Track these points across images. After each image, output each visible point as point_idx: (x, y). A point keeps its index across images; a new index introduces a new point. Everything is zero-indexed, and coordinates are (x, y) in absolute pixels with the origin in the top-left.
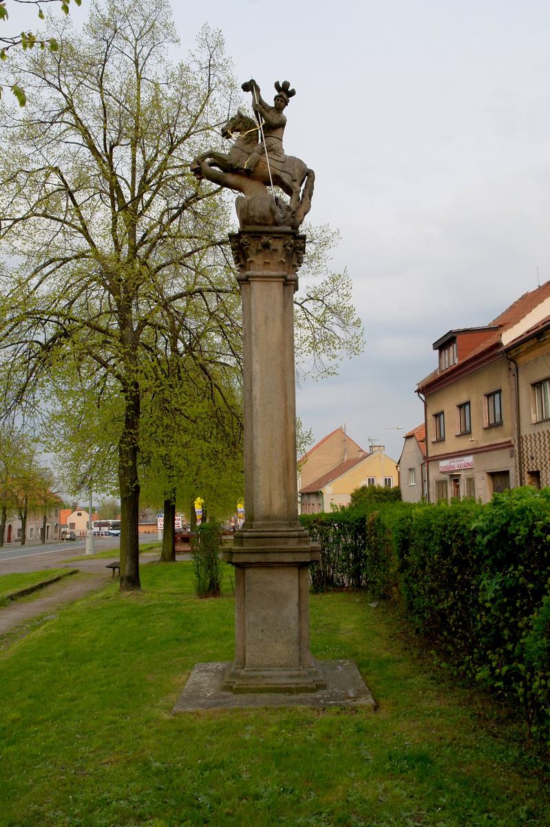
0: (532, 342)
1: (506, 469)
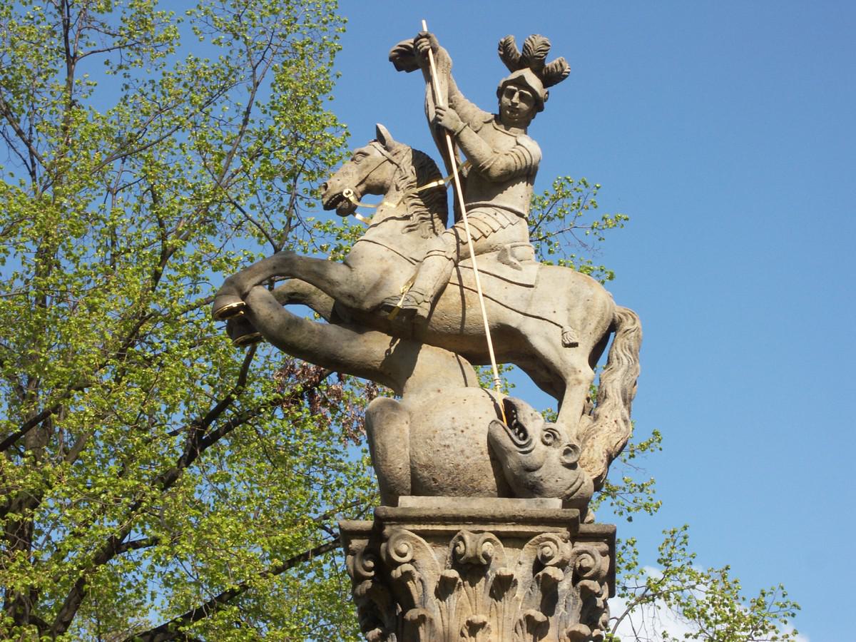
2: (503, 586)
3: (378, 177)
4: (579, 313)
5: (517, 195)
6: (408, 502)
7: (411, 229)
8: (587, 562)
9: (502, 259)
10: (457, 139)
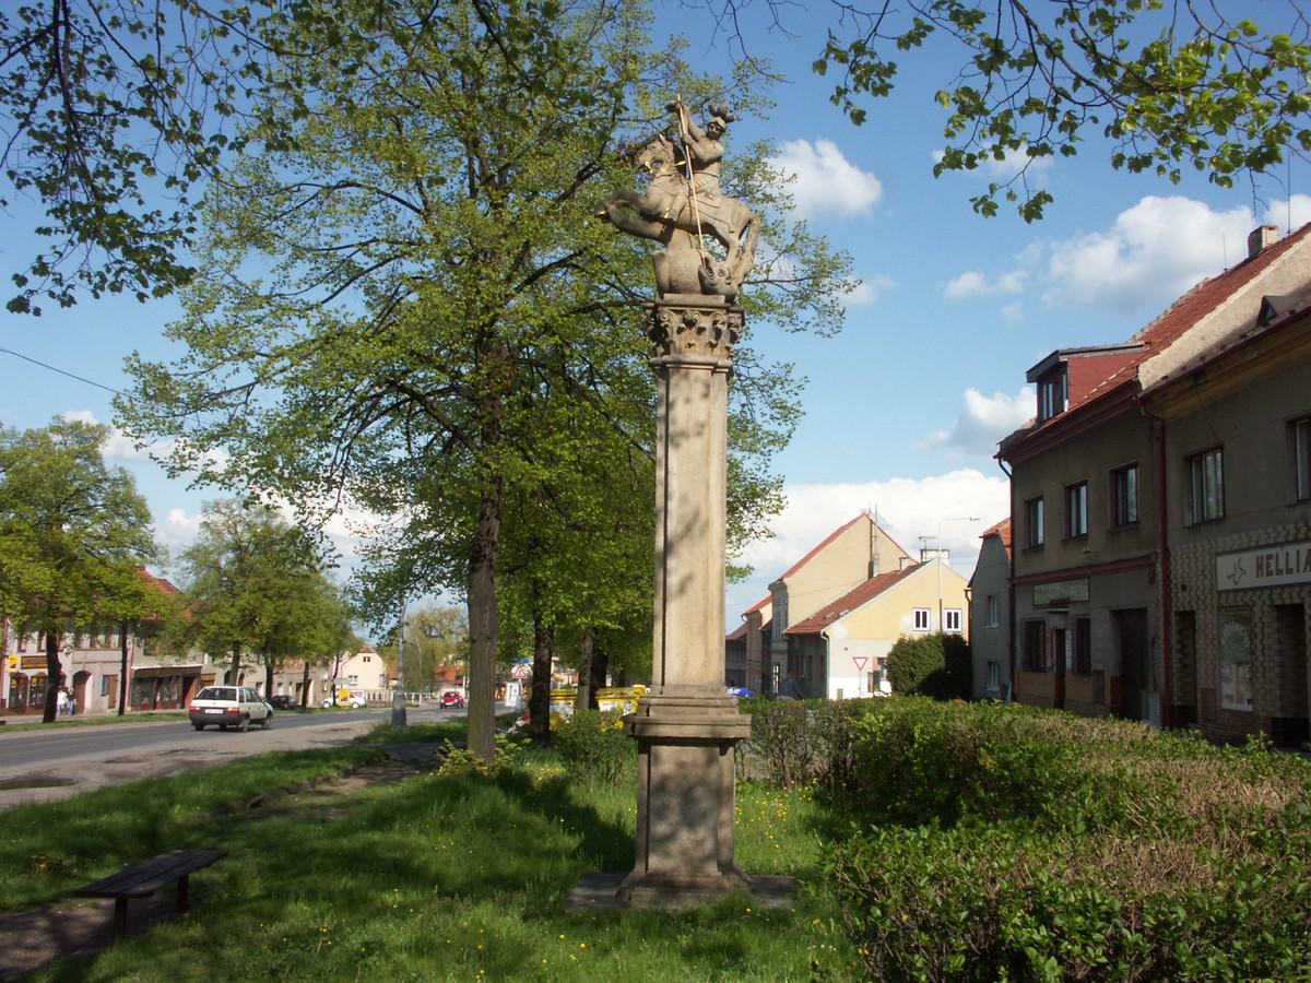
0: (1186, 385)
1: (1144, 606)
2: (701, 331)
3: (659, 157)
4: (735, 219)
5: (714, 169)
6: (667, 296)
7: (671, 180)
8: (733, 321)
9: (707, 196)
10: (690, 147)
